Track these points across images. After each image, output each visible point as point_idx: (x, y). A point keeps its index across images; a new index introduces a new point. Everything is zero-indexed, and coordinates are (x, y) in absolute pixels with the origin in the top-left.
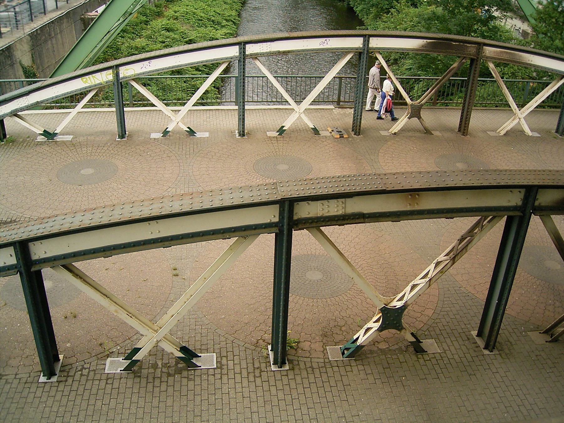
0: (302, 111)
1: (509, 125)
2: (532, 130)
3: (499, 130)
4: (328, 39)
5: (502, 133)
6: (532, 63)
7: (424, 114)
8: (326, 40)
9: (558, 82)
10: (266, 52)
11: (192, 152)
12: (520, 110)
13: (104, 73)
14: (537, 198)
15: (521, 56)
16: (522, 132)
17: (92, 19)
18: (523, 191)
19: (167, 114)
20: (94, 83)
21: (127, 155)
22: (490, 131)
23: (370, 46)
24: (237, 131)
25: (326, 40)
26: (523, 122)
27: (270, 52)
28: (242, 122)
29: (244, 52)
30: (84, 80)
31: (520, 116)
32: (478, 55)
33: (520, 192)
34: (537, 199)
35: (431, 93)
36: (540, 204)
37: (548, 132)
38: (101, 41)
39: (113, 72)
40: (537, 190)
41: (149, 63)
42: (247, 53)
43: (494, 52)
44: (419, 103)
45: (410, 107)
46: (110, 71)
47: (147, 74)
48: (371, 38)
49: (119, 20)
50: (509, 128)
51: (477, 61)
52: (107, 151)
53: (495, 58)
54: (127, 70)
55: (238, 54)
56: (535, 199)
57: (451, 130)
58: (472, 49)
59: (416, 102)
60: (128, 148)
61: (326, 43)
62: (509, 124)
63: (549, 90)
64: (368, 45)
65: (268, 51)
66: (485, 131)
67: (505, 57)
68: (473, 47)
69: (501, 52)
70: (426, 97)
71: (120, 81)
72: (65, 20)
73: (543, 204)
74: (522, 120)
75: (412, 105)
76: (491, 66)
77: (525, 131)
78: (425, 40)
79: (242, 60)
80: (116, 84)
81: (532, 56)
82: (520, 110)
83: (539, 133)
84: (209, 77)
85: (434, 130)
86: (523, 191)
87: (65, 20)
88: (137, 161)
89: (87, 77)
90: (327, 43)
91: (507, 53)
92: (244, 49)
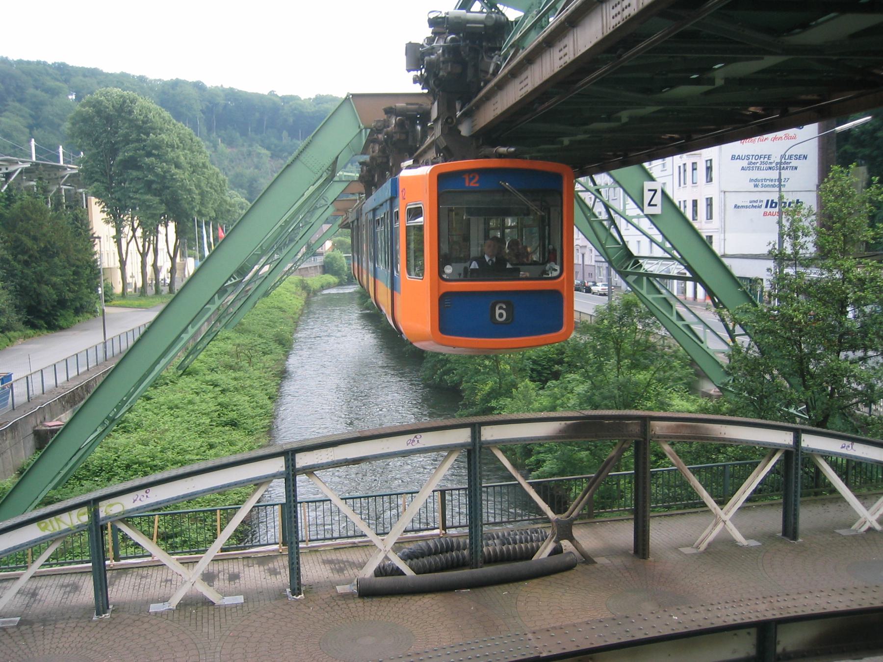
0: (389, 548)
1: (712, 534)
2: (747, 537)
3: (698, 541)
4: (418, 435)
5: (703, 547)
6: (726, 436)
7: (577, 533)
8: (416, 437)
9: (770, 459)
10: (327, 463)
11: (219, 629)
12: (722, 509)
13: (75, 513)
14: (778, 640)
15: (707, 429)
16: (733, 542)
17: (53, 432)
18: (753, 631)
19: (175, 570)
20: (58, 530)
21: (111, 643)
22: (683, 546)
23: (483, 439)
24: (288, 590)
25: (416, 437)
26: (731, 526)
27: (333, 461)
28: (295, 574)
29: (294, 465)
30: (43, 525)
31: (727, 518)
32: (646, 435)
33: (749, 633)
34: (779, 642)
35: (584, 499)
36: (784, 650)
37: (771, 536)
38: (67, 464)
39: (89, 510)
40: (776, 628)
41: (146, 492)
42: (298, 466)
43: (668, 427)
44: (568, 517)
45: (554, 524)
46: (85, 509)
47: (142, 510)
48: (482, 428)
49: (96, 430)
50: (711, 538)
51: (645, 444)
52: (79, 639)
53: (671, 437)
54: (112, 505)
55: (284, 469)
56: (775, 643)
57: (624, 553)
58: (635, 428)
59: (562, 517)
60: (113, 631)
61: (416, 442)
62: (711, 532)
63: (759, 473)
64: (480, 438)
65: (329, 460)
66: (676, 549)
67: (685, 432)
68: (635, 424)
69: (678, 426)
70: (577, 506)
71: (101, 523)
72: (9, 435)
73: (789, 649)
74: (729, 523)
75: (557, 521)
76: (667, 448)
77: (737, 540)
78: (563, 423)
79: (291, 478)
80: (94, 529)
81: (724, 426)
82: (722, 509)
83: (758, 541)
84: (202, 557)
85: (597, 556)
86: (753, 631)
87: (9, 435)
88: (128, 652)
89: (47, 520)
90: (418, 441)
91: (687, 426)
92: (294, 460)
